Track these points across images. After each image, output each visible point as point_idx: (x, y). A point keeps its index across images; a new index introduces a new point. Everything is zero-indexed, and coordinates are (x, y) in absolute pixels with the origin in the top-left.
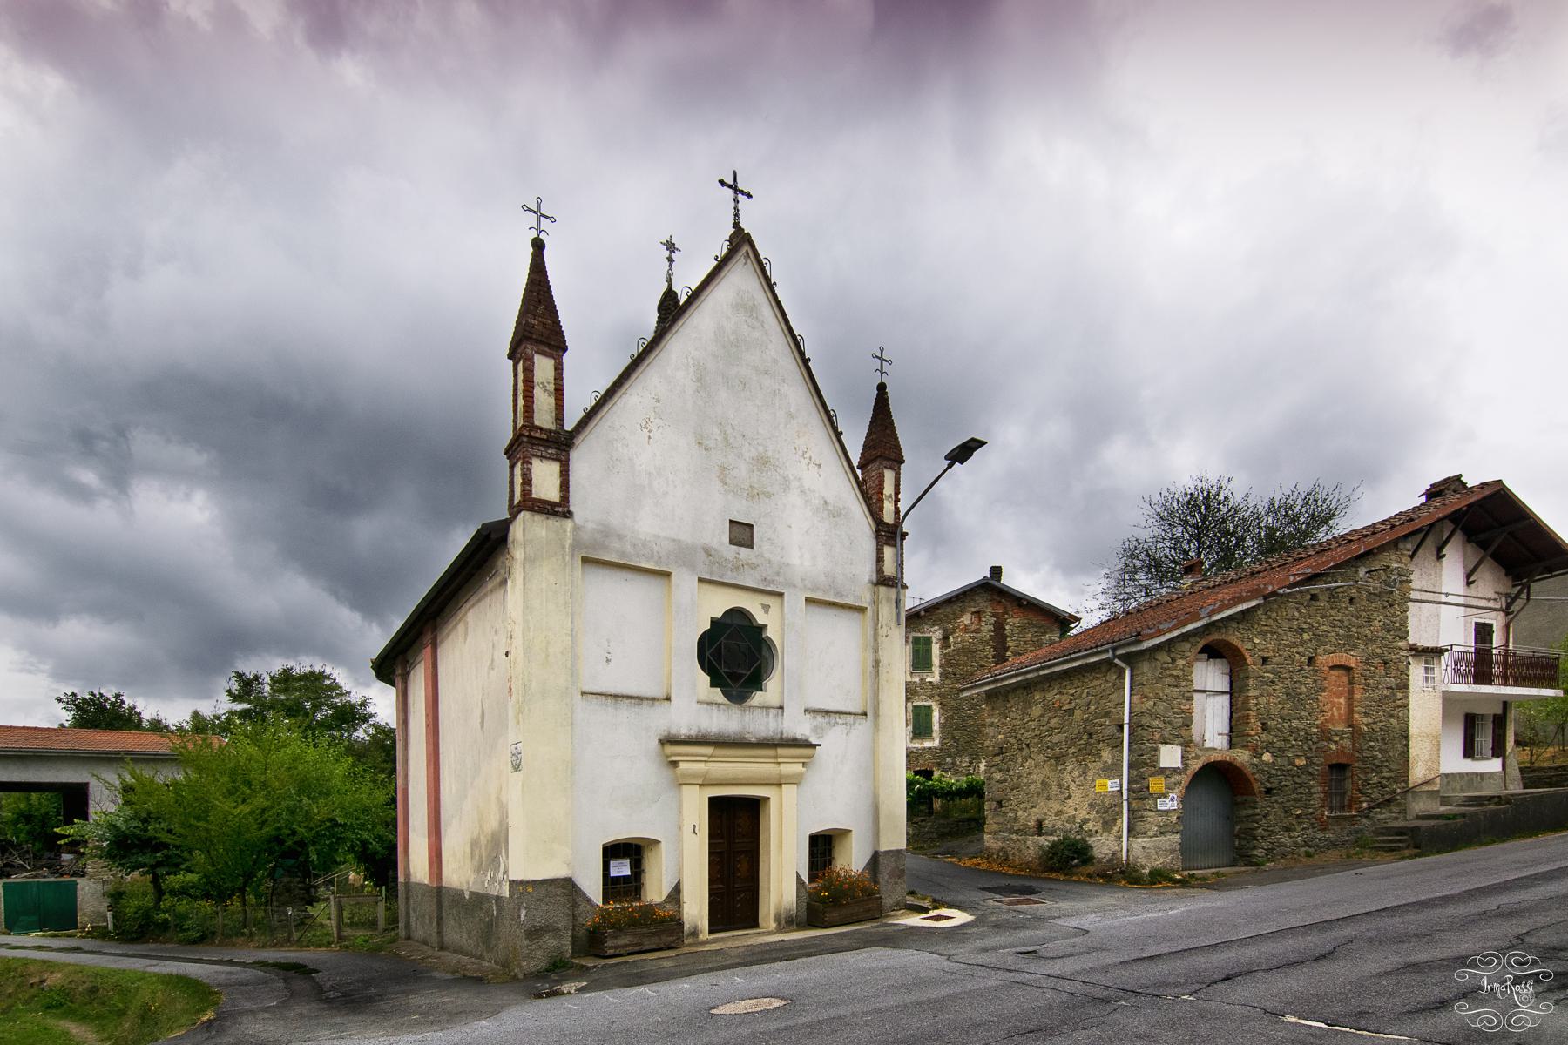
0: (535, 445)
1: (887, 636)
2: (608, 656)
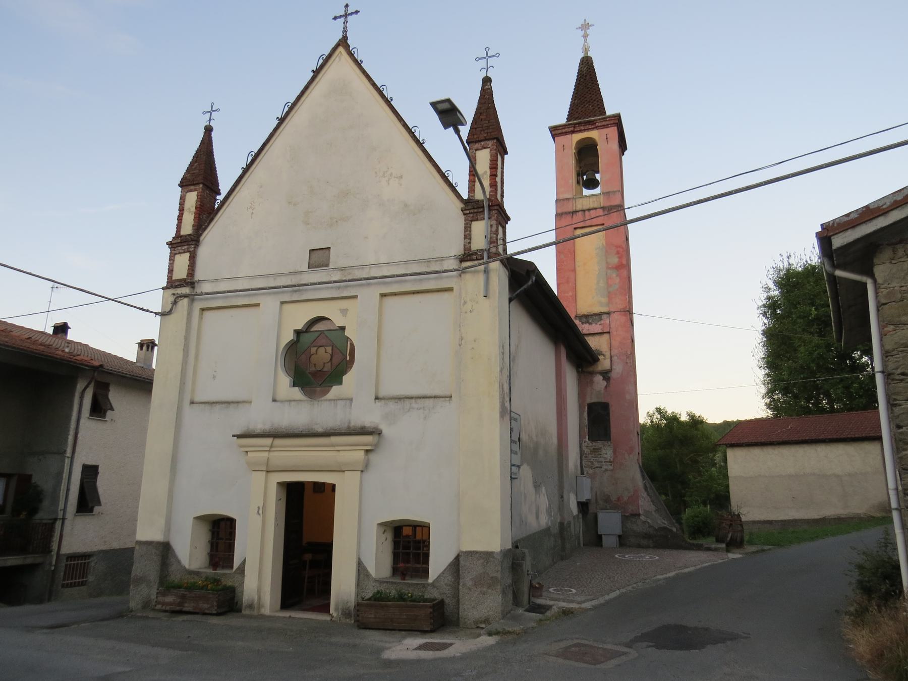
0: (175, 247)
1: (471, 311)
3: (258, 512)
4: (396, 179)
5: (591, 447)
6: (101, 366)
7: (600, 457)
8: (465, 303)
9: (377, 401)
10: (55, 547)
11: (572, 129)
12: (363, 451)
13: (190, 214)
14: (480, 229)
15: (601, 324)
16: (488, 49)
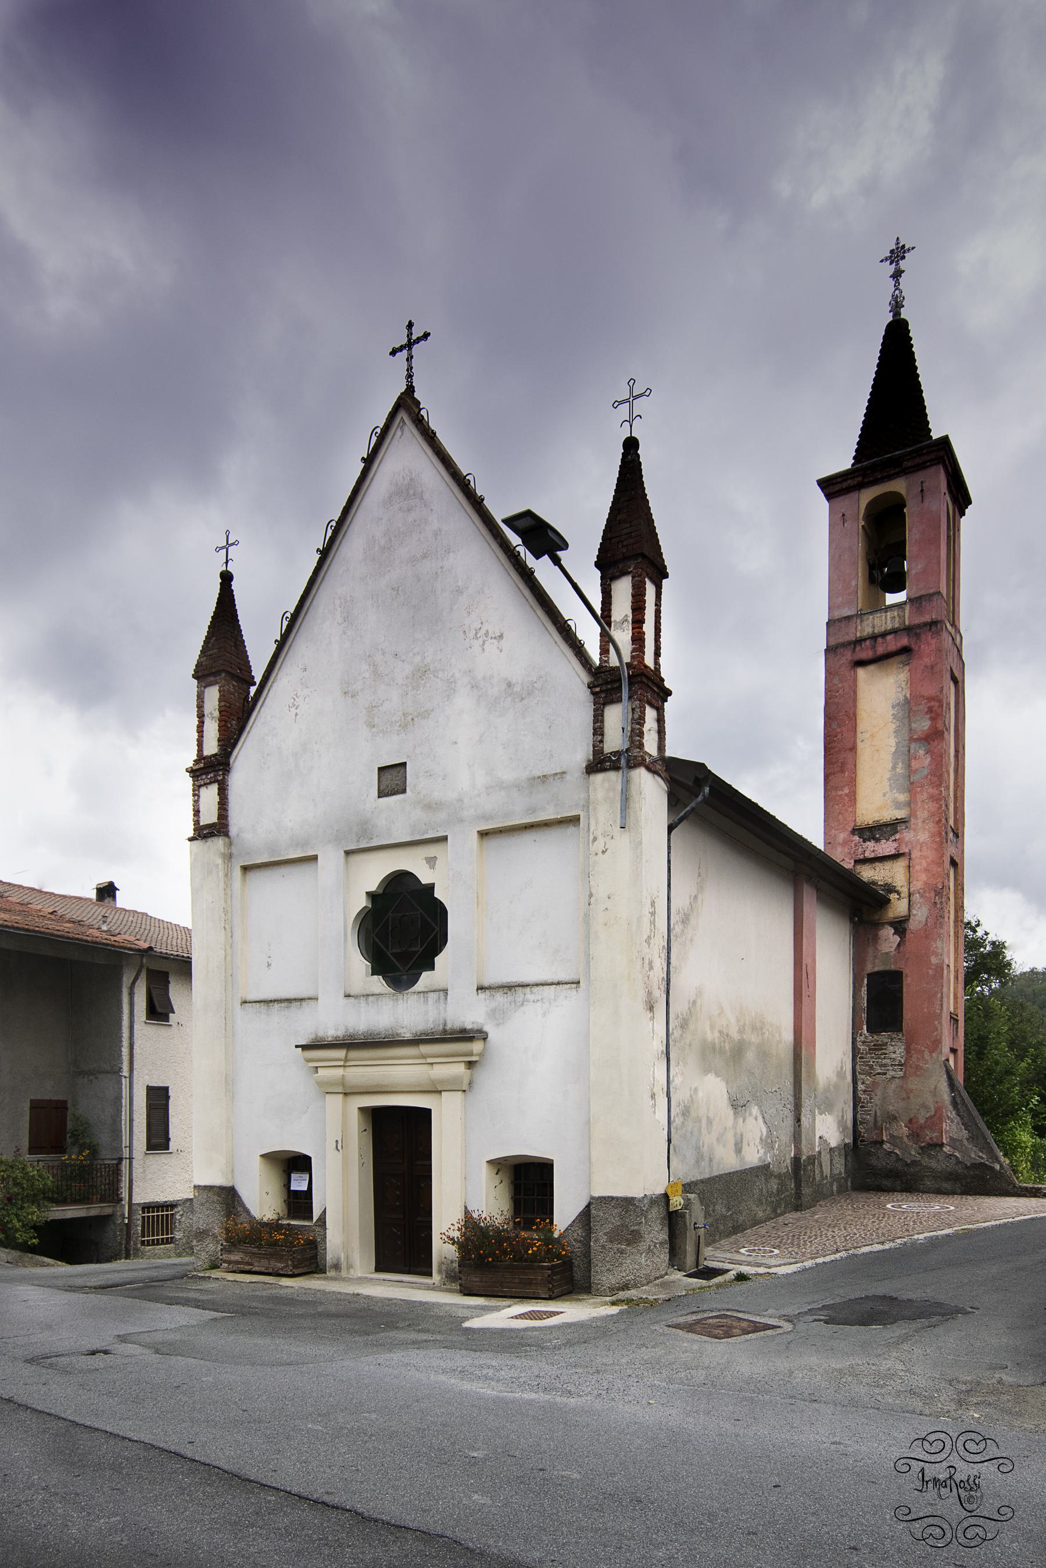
0: (198, 776)
1: (603, 852)
2: (269, 960)
3: (337, 1147)
4: (493, 640)
5: (872, 1041)
6: (151, 948)
7: (885, 1058)
8: (595, 839)
9: (480, 991)
10: (125, 1194)
11: (860, 479)
12: (463, 1065)
13: (214, 721)
14: (615, 716)
15: (895, 840)
16: (632, 381)
